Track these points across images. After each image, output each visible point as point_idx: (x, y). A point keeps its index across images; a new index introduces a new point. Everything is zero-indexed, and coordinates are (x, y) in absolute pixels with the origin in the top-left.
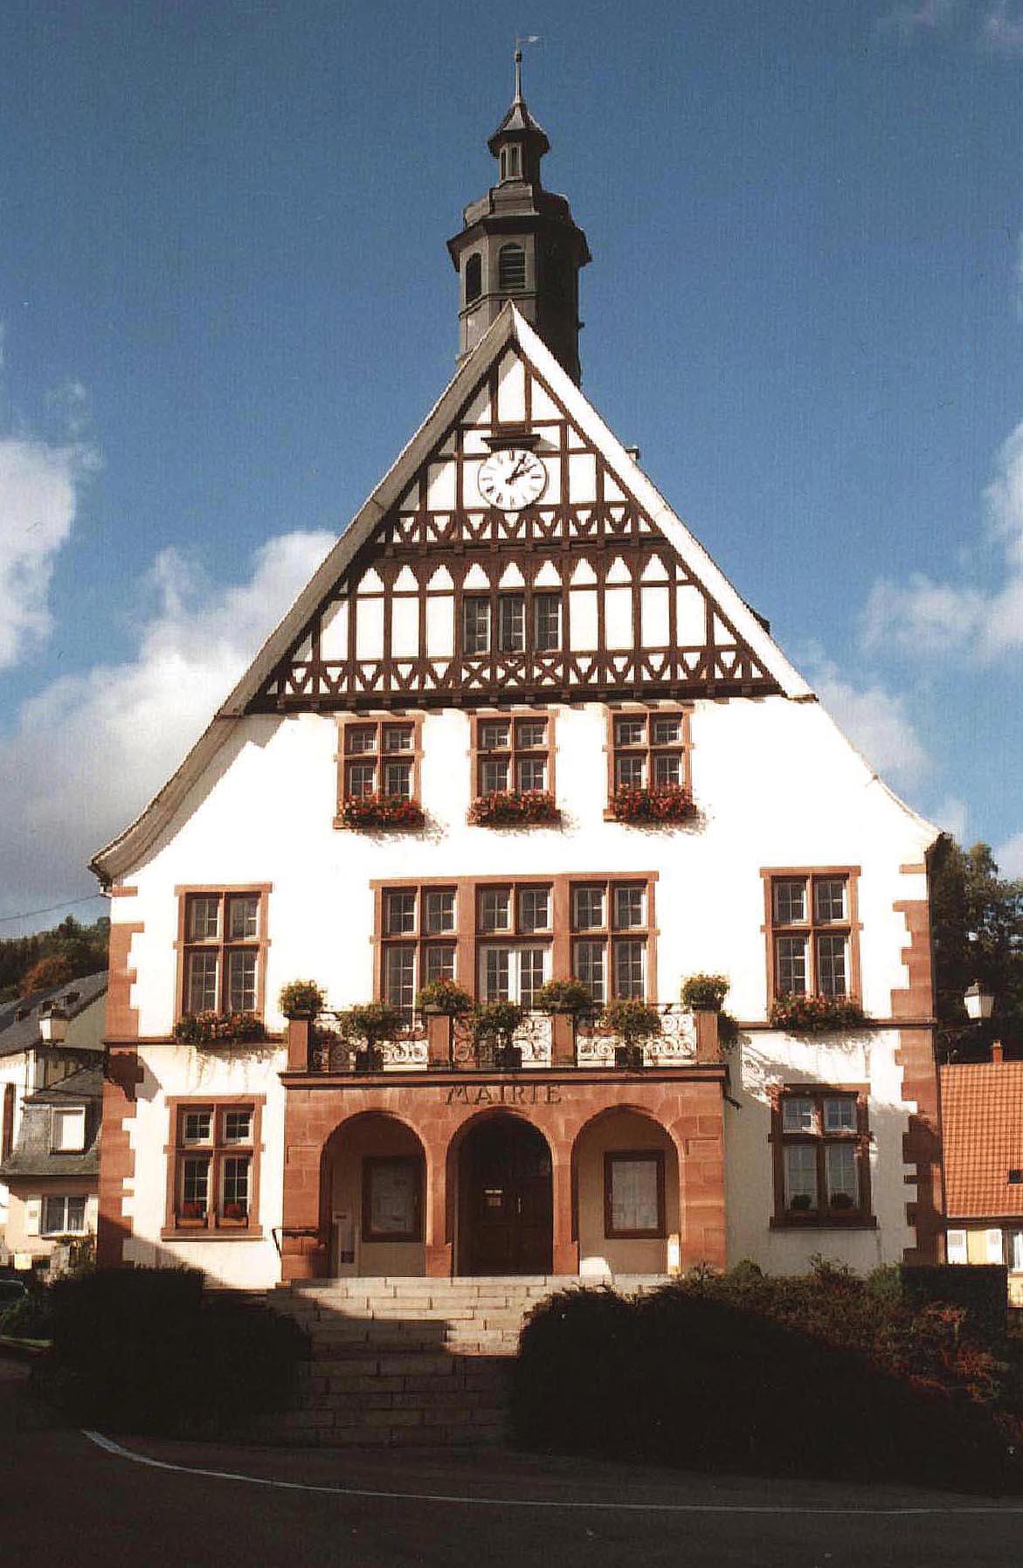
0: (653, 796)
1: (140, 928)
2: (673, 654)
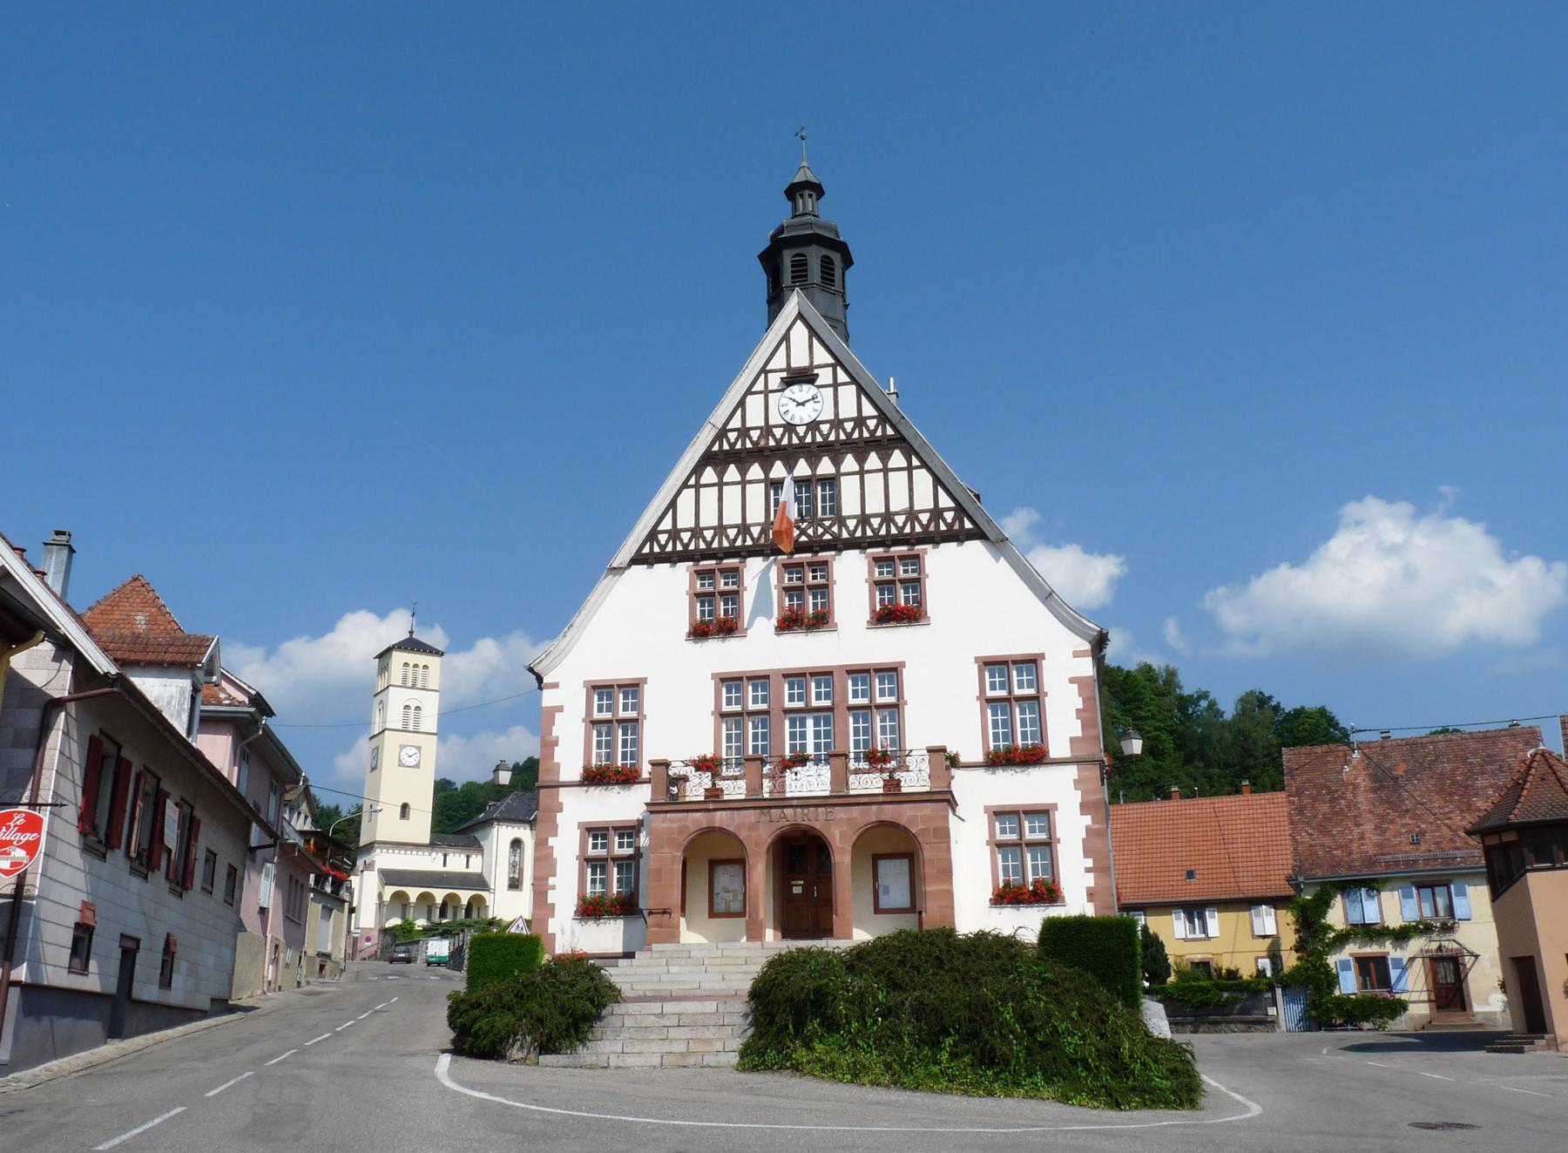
0: (899, 609)
1: (560, 709)
2: (912, 515)
